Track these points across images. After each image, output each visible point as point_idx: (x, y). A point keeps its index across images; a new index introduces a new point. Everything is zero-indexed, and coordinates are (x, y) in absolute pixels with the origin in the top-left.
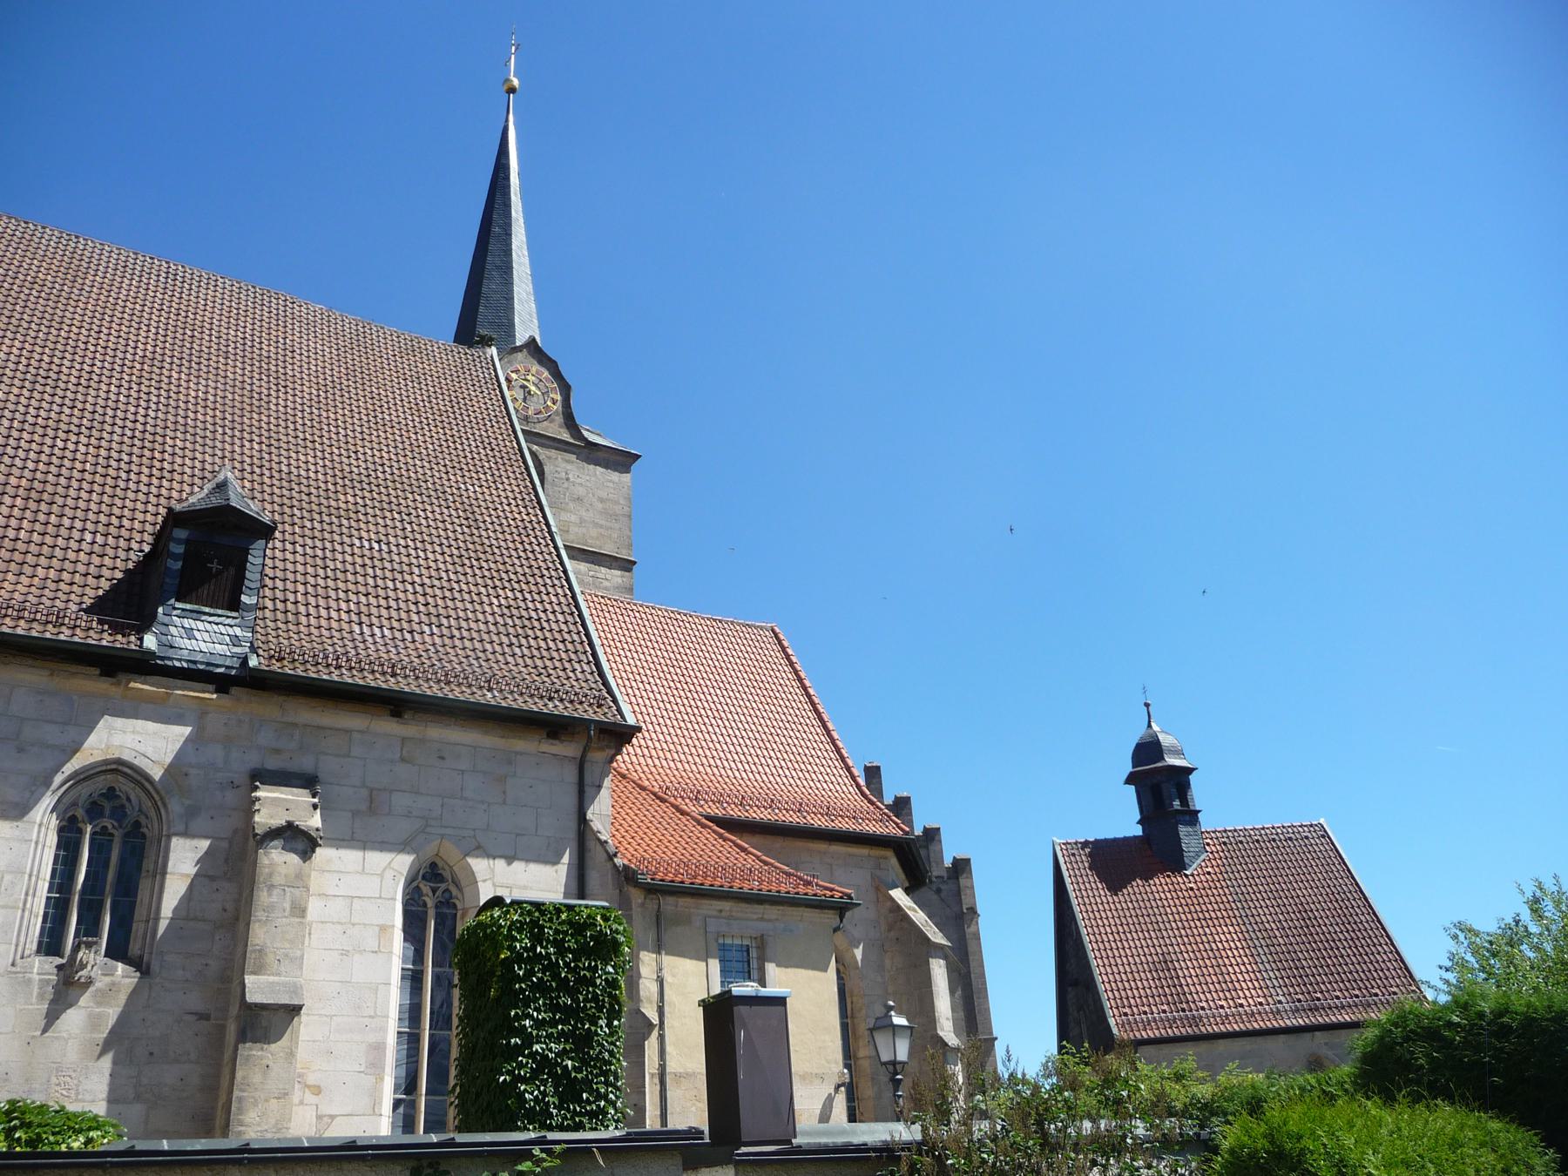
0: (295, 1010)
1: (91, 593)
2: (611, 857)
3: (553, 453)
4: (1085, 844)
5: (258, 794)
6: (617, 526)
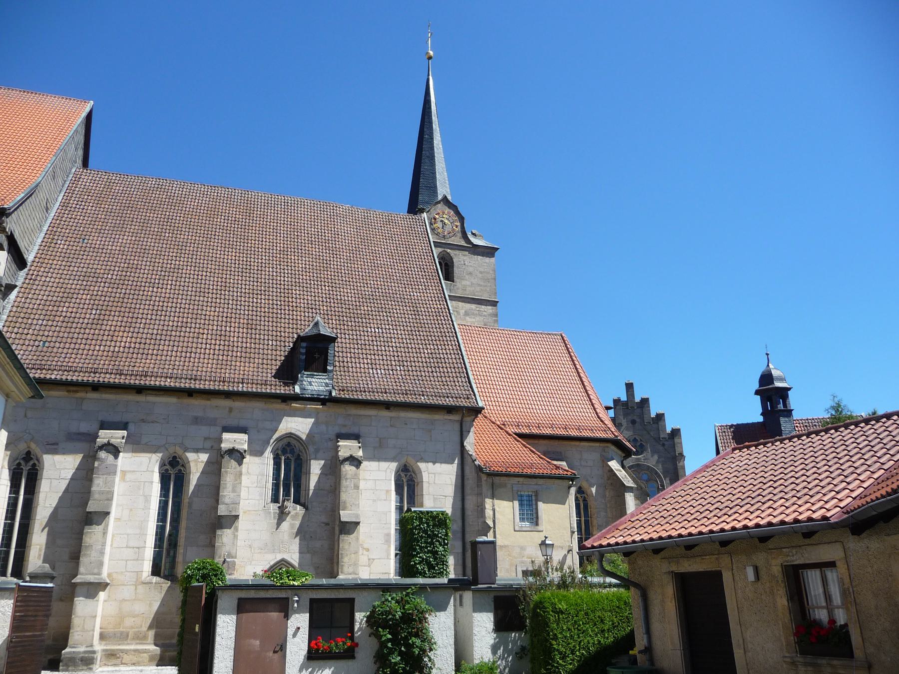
0: (358, 523)
1: (274, 367)
2: (474, 461)
3: (457, 252)
4: (731, 426)
5: (339, 444)
6: (489, 284)
